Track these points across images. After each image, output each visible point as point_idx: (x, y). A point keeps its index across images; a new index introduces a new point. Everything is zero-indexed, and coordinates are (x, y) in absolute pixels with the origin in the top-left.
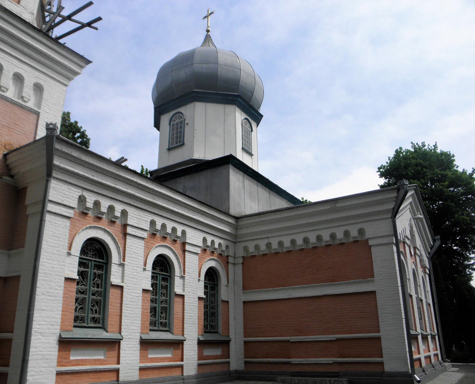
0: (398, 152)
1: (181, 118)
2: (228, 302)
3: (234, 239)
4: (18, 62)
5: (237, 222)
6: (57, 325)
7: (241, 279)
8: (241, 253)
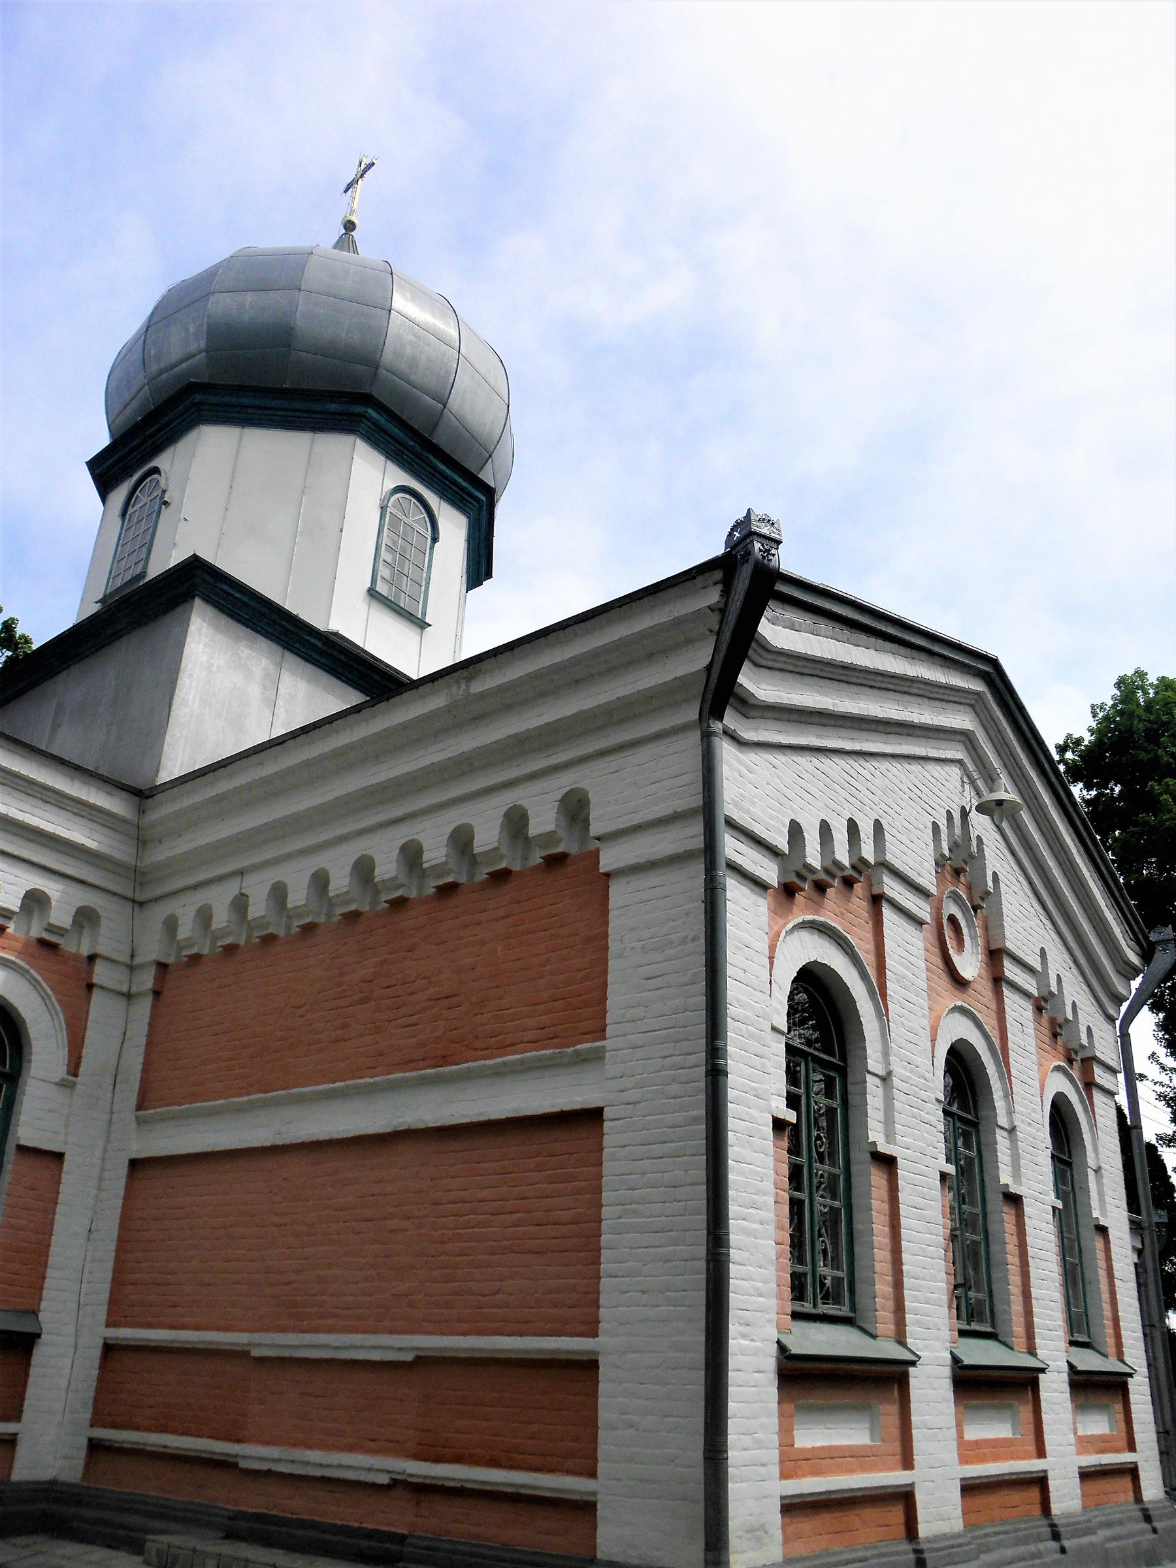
0: (1127, 687)
2: (59, 1157)
3: (137, 886)
5: (142, 811)
6: (760, 1445)
7: (141, 1059)
8: (152, 949)
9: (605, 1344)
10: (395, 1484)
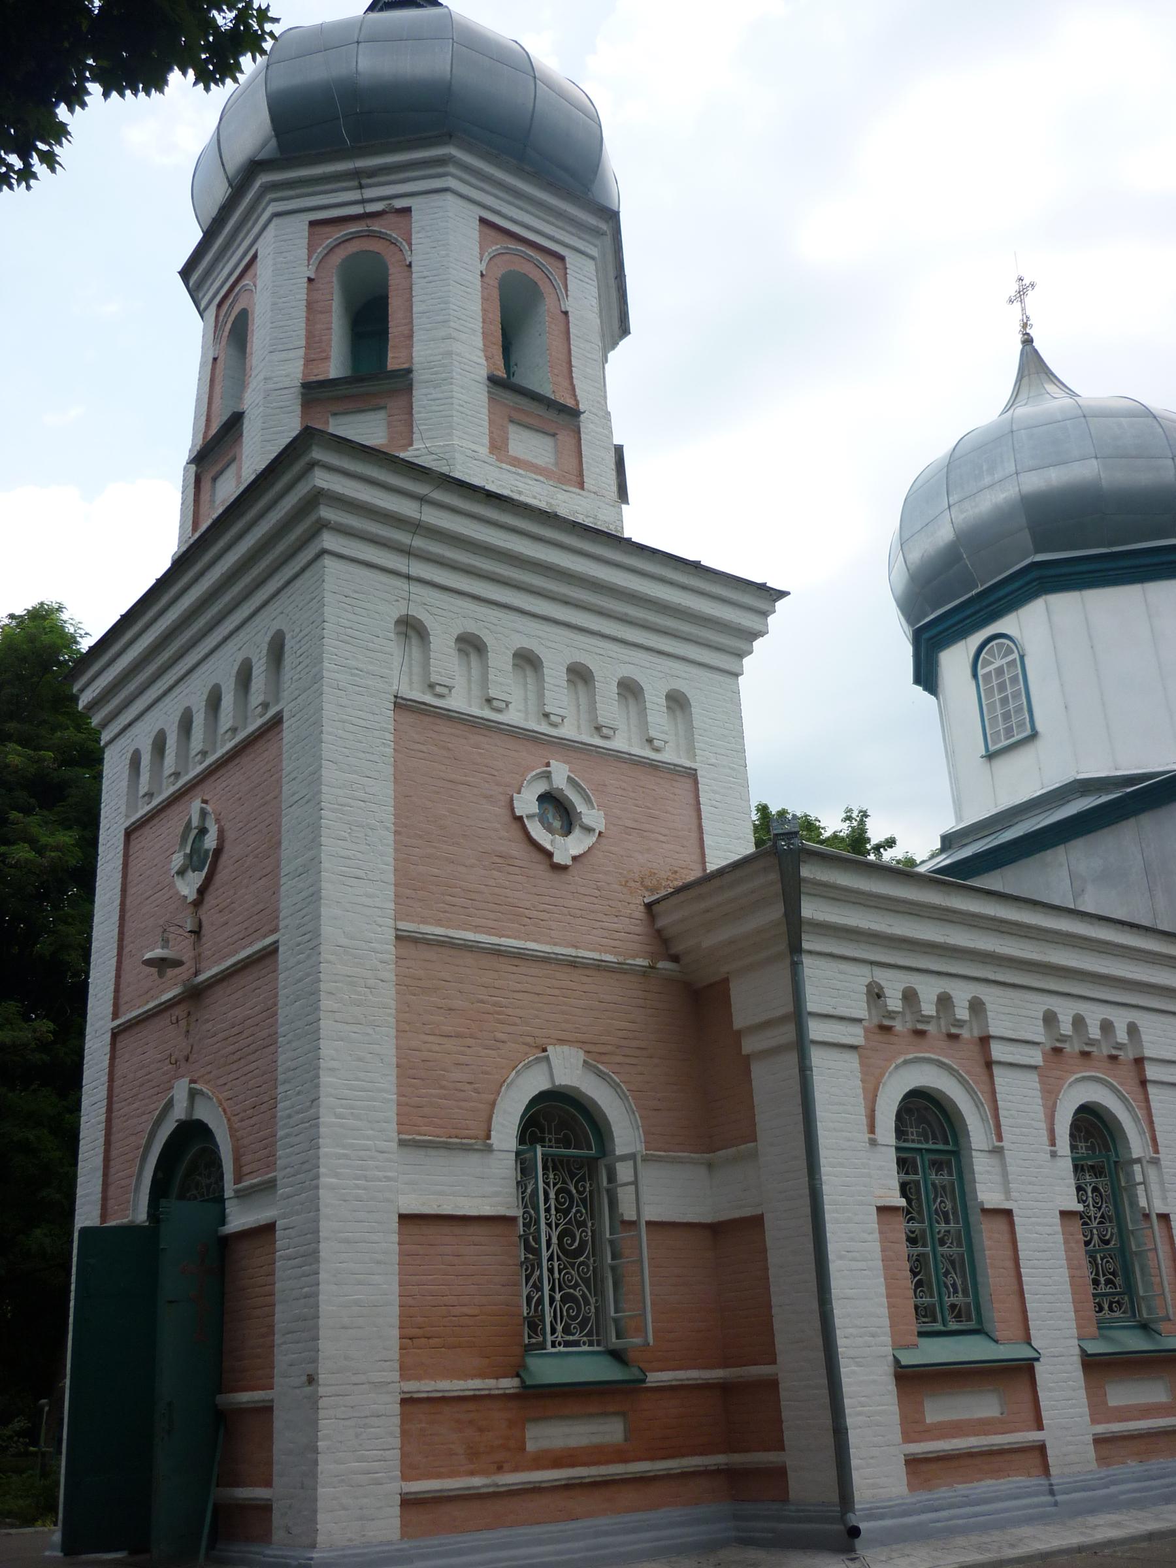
1: (1009, 651)
4: (619, 650)
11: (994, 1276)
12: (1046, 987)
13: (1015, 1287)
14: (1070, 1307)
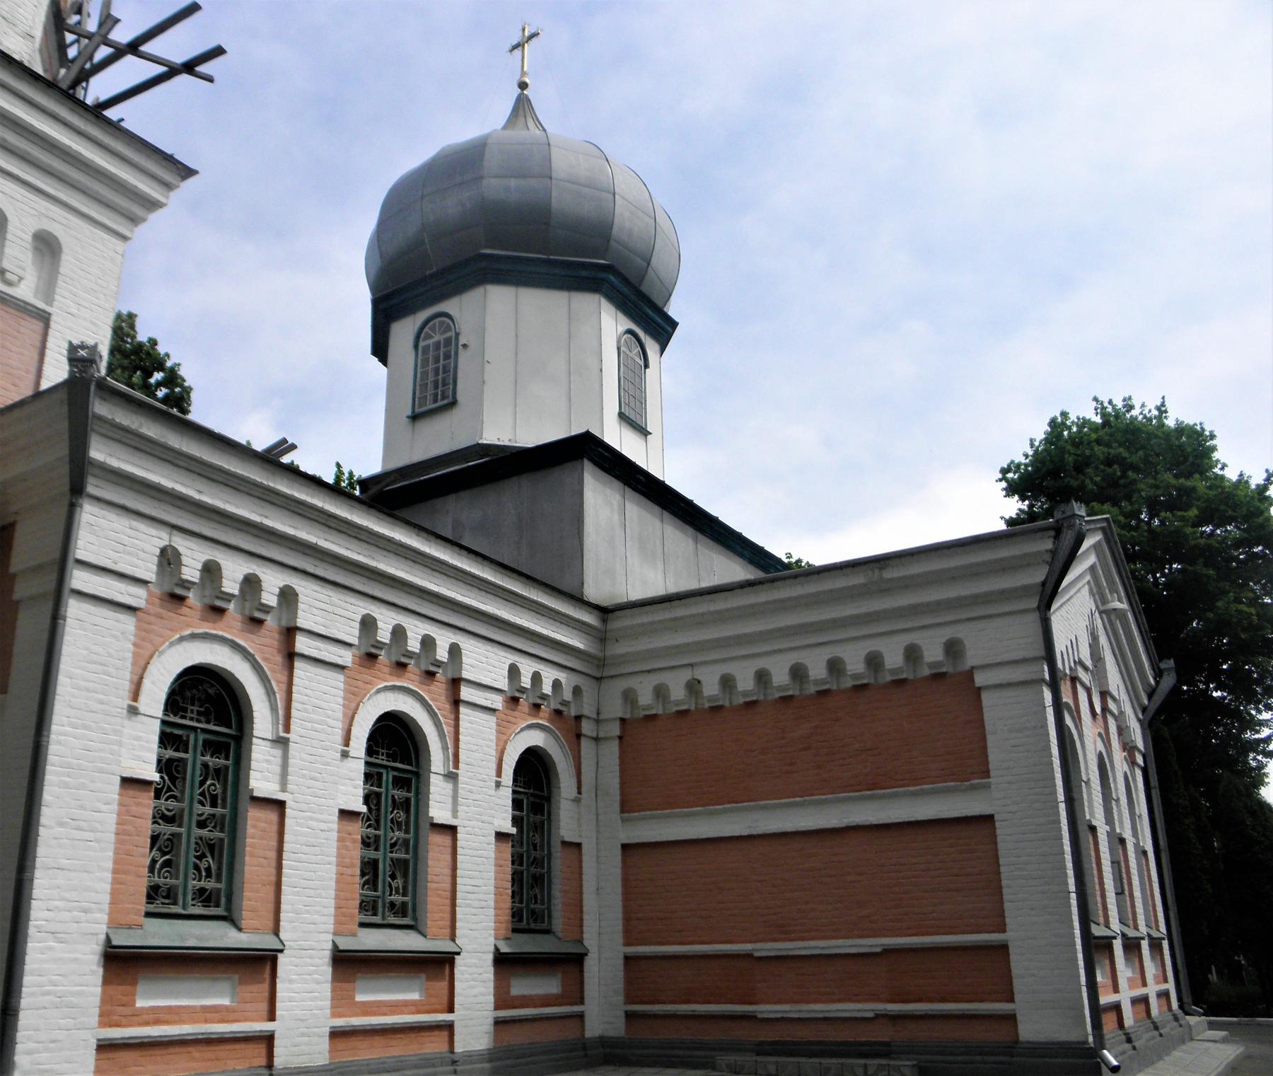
0: (1056, 426)
1: (448, 329)
2: (579, 845)
3: (598, 668)
5: (604, 621)
7: (617, 780)
9: (1009, 936)
10: (877, 1016)
11: (254, 865)
12: (370, 591)
13: (273, 878)
14: (331, 903)
